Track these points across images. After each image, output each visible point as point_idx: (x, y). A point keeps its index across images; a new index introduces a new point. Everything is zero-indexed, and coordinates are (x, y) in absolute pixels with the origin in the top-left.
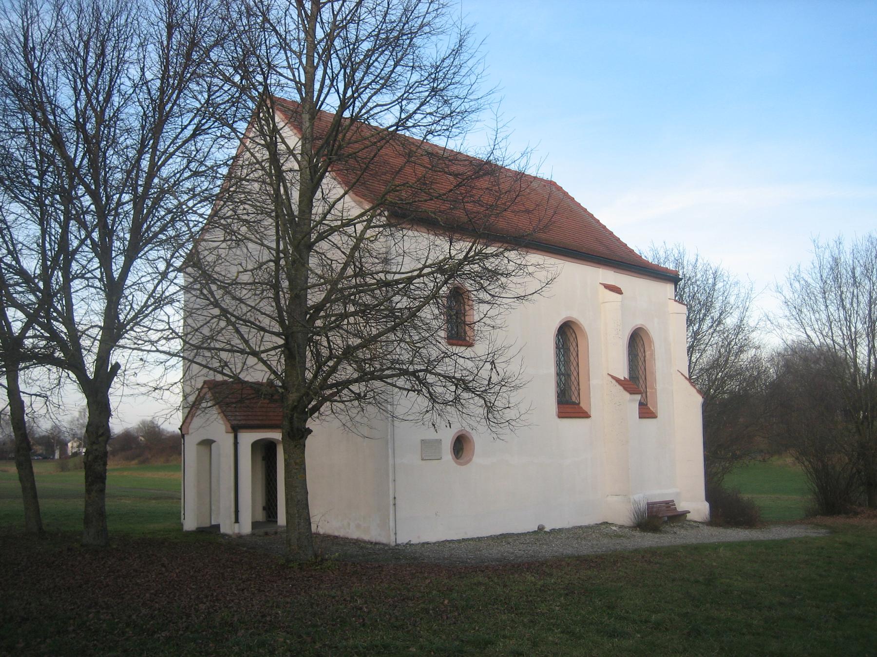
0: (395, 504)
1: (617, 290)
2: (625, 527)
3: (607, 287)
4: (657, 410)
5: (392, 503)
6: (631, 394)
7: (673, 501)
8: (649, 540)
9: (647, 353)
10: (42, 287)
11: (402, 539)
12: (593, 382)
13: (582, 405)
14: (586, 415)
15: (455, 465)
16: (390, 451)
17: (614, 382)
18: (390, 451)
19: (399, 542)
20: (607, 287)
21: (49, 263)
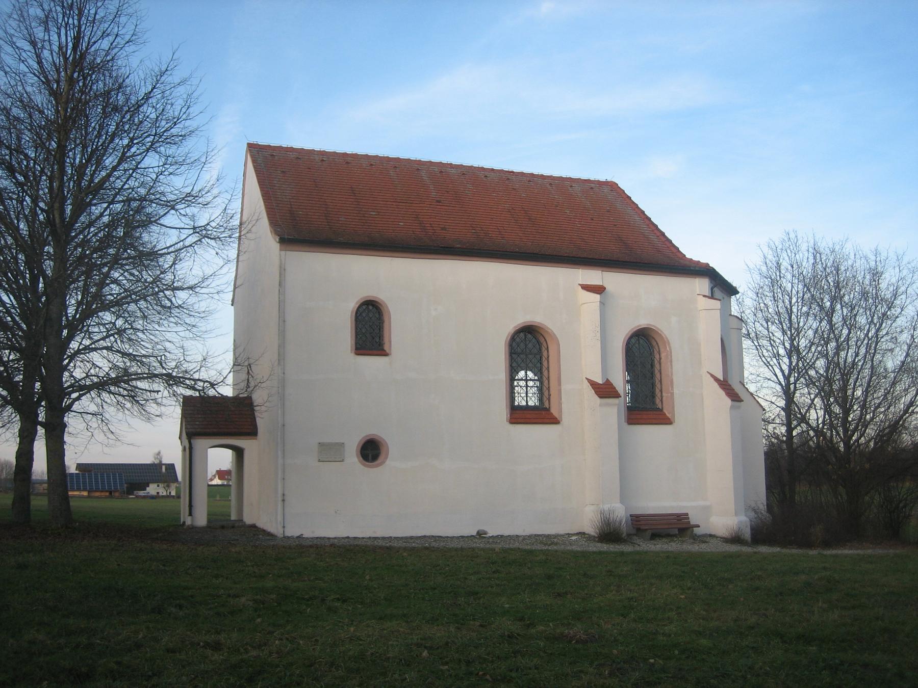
0: (283, 500)
1: (598, 290)
2: (590, 538)
3: (587, 288)
4: (674, 415)
5: (280, 499)
6: (601, 397)
7: (687, 514)
8: (605, 547)
9: (663, 355)
10: (49, 272)
11: (293, 531)
12: (566, 387)
13: (665, 411)
14: (667, 421)
15: (362, 467)
16: (280, 453)
17: (712, 379)
18: (280, 453)
19: (288, 534)
20: (587, 288)
21: (49, 249)
